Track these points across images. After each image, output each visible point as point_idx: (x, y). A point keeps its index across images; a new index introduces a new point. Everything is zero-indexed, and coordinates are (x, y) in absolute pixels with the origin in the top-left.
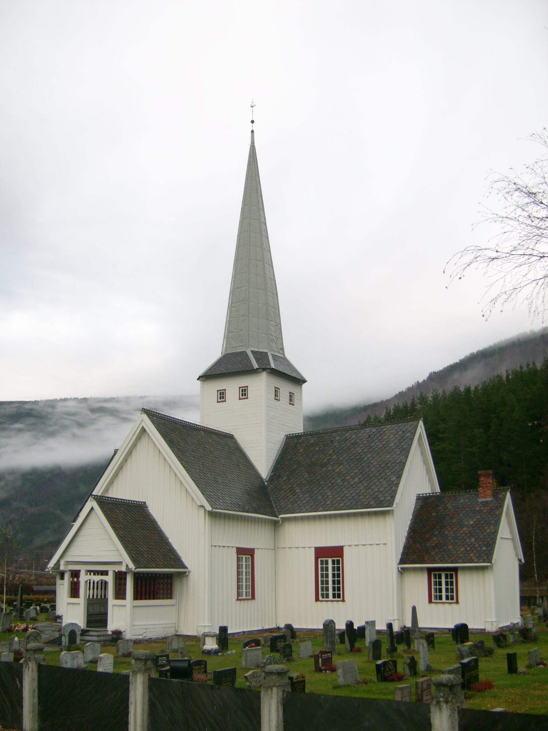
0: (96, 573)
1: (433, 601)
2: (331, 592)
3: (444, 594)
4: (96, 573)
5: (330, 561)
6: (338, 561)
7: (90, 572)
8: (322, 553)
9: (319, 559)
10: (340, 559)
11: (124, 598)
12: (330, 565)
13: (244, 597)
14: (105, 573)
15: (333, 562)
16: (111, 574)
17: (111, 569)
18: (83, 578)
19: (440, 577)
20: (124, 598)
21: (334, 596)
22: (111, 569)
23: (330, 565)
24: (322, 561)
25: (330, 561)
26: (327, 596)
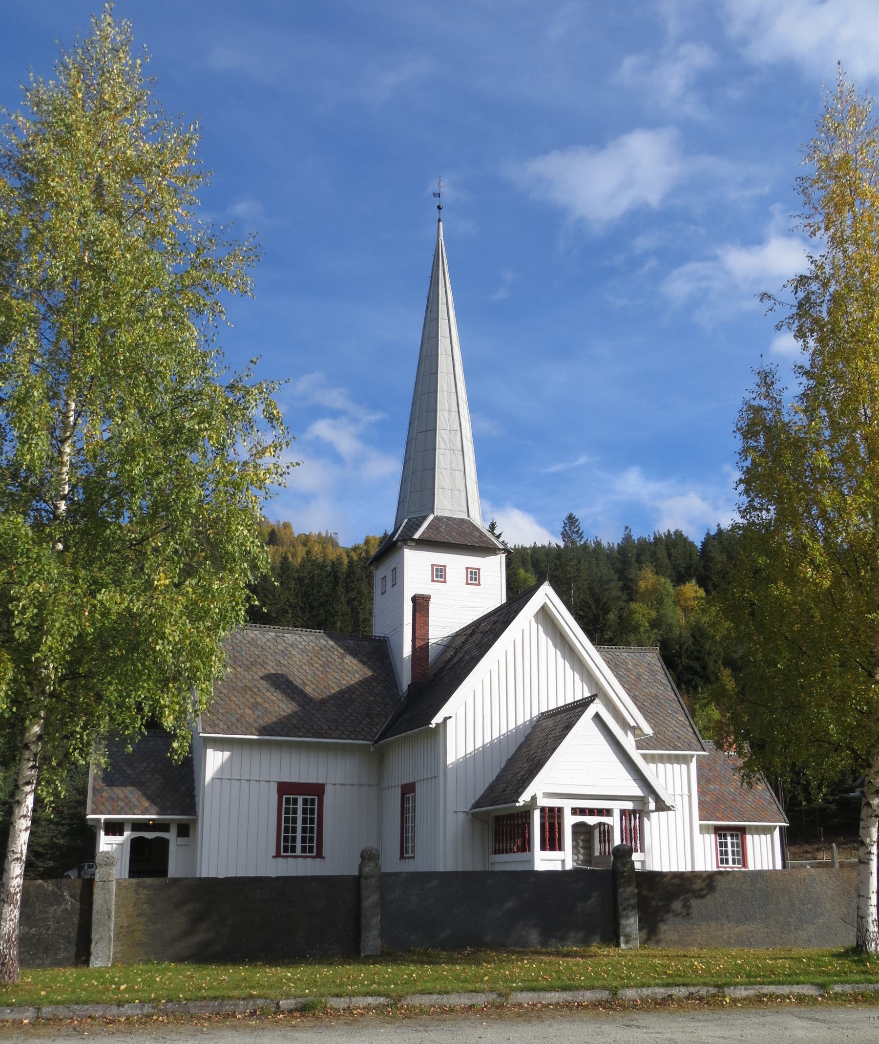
0: (592, 812)
1: (282, 854)
2: (299, 844)
3: (299, 844)
4: (592, 812)
5: (300, 799)
6: (313, 801)
7: (576, 811)
8: (284, 788)
9: (285, 797)
10: (316, 798)
11: (560, 848)
12: (300, 806)
13: (789, 862)
14: (608, 812)
15: (305, 802)
16: (617, 814)
17: (617, 806)
18: (569, 821)
19: (295, 802)
20: (560, 848)
21: (303, 850)
22: (617, 806)
23: (300, 806)
24: (288, 800)
25: (300, 799)
26: (293, 849)
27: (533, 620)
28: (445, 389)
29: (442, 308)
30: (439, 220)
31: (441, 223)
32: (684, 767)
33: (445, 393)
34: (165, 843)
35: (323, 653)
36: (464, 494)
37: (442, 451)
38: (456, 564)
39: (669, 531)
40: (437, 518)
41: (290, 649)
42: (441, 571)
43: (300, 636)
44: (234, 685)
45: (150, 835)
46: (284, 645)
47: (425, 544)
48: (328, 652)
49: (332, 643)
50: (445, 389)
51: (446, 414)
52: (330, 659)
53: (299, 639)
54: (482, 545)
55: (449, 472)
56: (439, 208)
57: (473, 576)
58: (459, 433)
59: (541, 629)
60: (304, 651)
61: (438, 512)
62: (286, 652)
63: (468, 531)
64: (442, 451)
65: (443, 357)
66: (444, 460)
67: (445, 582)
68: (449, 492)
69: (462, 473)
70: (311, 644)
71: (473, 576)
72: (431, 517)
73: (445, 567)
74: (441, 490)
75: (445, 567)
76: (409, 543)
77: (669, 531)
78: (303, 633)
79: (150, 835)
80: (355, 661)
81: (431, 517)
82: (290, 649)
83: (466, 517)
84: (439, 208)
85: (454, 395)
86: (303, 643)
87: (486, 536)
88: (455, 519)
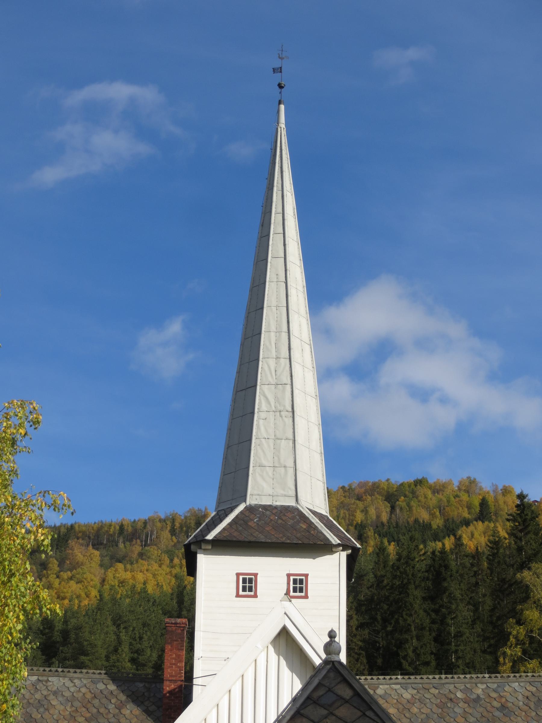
27: (271, 649)
28: (273, 328)
29: (276, 218)
30: (280, 103)
31: (282, 107)
33: (273, 334)
35: (96, 702)
36: (291, 471)
37: (263, 415)
38: (274, 571)
39: (527, 496)
40: (250, 509)
41: (51, 697)
42: (251, 581)
43: (71, 680)
44: (452, 696)
46: (45, 693)
47: (226, 545)
48: (104, 701)
49: (112, 687)
50: (273, 328)
51: (272, 363)
52: (102, 710)
53: (68, 683)
54: (306, 541)
55: (271, 442)
56: (280, 86)
57: (298, 586)
58: (288, 387)
59: (283, 662)
60: (71, 700)
61: (251, 500)
62: (45, 702)
63: (291, 522)
64: (263, 415)
65: (274, 285)
66: (264, 425)
67: (255, 596)
68: (270, 471)
69: (291, 443)
70: (83, 690)
71: (298, 586)
72: (241, 507)
73: (256, 575)
74: (258, 469)
75: (256, 575)
76: (204, 546)
77: (112, 521)
78: (76, 675)
80: (137, 711)
81: (241, 507)
82: (51, 697)
83: (292, 503)
84: (280, 86)
85: (285, 336)
86: (72, 690)
87: (316, 528)
88: (276, 507)
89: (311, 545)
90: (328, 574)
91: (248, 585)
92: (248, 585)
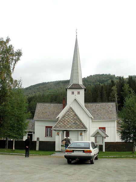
5: (49, 129)
32: (114, 122)
34: (32, 134)
38: (76, 91)
45: (30, 133)
79: (30, 133)
89: (81, 88)
90: (82, 92)
91: (73, 93)
92: (73, 93)
